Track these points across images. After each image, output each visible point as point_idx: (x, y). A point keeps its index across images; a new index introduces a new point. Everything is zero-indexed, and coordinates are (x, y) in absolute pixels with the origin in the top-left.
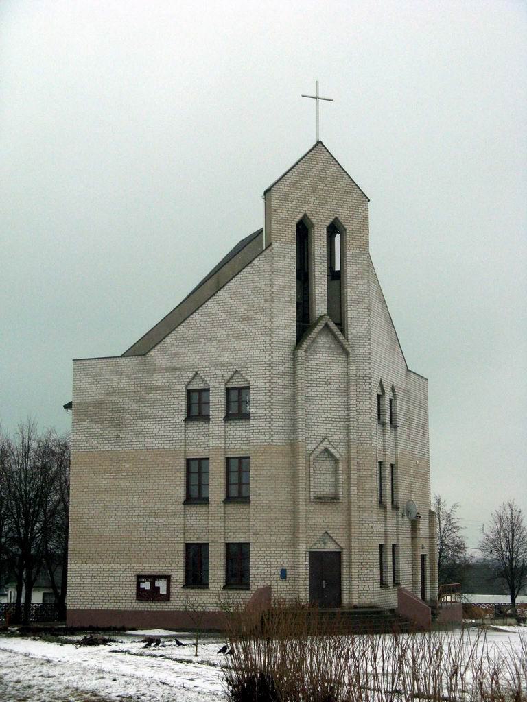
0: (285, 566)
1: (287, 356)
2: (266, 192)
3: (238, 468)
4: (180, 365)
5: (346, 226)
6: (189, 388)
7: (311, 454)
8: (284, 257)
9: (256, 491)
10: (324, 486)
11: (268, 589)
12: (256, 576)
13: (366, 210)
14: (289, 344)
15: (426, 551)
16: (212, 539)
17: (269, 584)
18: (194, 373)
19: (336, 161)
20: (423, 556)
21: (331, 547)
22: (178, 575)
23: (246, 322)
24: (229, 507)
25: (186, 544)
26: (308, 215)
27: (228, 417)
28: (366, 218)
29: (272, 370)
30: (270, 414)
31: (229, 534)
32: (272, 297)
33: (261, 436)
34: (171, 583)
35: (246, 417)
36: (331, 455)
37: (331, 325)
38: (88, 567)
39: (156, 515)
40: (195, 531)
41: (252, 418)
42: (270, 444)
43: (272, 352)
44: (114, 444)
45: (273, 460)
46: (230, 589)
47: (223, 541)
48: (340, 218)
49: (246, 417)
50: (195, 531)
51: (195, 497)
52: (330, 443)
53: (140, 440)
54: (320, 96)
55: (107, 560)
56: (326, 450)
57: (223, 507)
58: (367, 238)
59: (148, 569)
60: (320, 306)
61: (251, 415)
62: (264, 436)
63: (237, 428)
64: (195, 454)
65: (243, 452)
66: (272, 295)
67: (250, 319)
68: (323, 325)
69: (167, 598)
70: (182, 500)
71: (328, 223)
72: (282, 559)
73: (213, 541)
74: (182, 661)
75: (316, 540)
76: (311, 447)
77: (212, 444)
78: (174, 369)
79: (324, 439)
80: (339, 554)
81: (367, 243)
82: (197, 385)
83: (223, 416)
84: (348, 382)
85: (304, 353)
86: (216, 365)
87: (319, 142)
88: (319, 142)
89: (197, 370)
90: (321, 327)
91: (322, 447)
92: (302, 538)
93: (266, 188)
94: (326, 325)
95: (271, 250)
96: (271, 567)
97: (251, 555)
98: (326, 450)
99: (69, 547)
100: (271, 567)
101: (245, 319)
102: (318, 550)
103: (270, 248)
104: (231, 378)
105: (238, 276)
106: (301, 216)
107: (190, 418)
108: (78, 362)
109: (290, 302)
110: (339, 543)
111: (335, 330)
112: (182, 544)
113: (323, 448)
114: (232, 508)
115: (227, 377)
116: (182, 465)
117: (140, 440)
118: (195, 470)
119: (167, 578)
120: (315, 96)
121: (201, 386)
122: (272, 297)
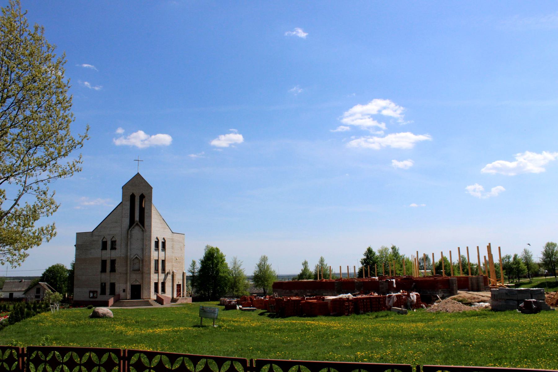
0: (125, 288)
2: (123, 187)
3: (113, 262)
10: (136, 267)
11: (119, 295)
15: (181, 283)
20: (179, 286)
21: (138, 283)
22: (99, 290)
24: (112, 273)
27: (111, 249)
28: (151, 193)
35: (115, 249)
36: (138, 259)
49: (115, 249)
51: (103, 270)
52: (138, 255)
56: (136, 257)
59: (92, 289)
60: (137, 218)
63: (113, 252)
70: (100, 271)
74: (482, 296)
82: (105, 240)
86: (109, 235)
91: (135, 257)
98: (136, 257)
107: (102, 249)
114: (112, 273)
115: (111, 238)
118: (104, 263)
119: (97, 292)
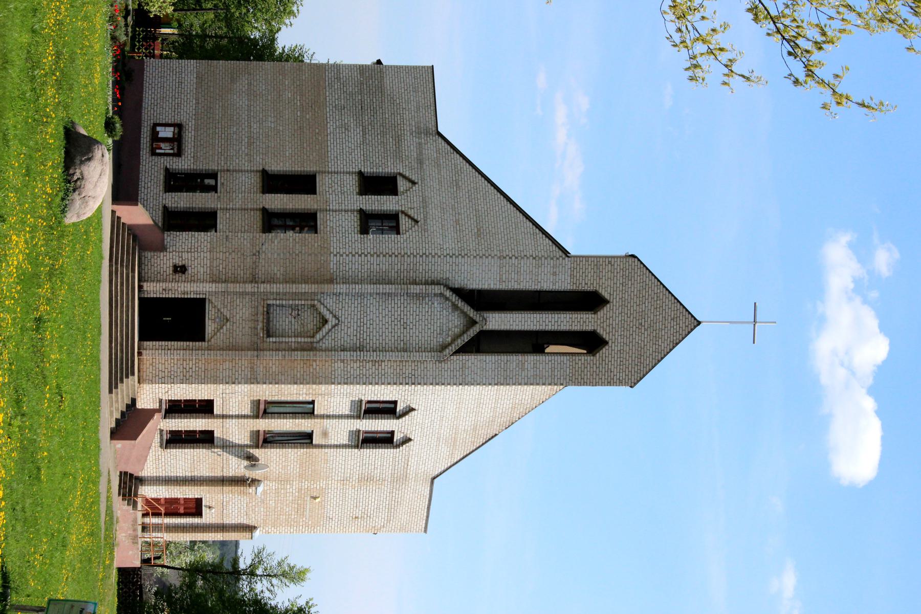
1: (437, 275)
2: (633, 256)
4: (425, 168)
5: (598, 355)
6: (398, 178)
7: (320, 302)
8: (554, 274)
9: (277, 238)
10: (283, 321)
12: (178, 238)
13: (621, 383)
14: (450, 278)
16: (222, 197)
17: (168, 250)
18: (416, 181)
19: (677, 344)
20: (195, 508)
22: (183, 164)
23: (476, 231)
24: (258, 214)
25: (217, 174)
26: (608, 305)
29: (418, 256)
30: (366, 253)
31: (228, 214)
32: (505, 258)
33: (341, 244)
34: (171, 158)
37: (474, 328)
38: (193, 78)
39: (250, 144)
40: (231, 181)
41: (362, 236)
42: (331, 253)
43: (440, 257)
44: (334, 105)
45: (313, 255)
46: (165, 177)
47: (219, 206)
48: (607, 347)
50: (231, 181)
52: (334, 327)
53: (338, 129)
54: (756, 325)
55: (200, 97)
56: (326, 321)
57: (258, 207)
58: (585, 384)
59: (189, 137)
60: (498, 321)
61: (365, 235)
62: (341, 247)
63: (353, 221)
64: (321, 182)
65: (322, 228)
66: (508, 258)
67: (479, 236)
68: (474, 318)
69: (153, 153)
70: (267, 168)
71: (600, 331)
72: (198, 263)
73: (219, 197)
75: (219, 307)
76: (329, 302)
77: (332, 197)
78: (420, 162)
79: (338, 319)
80: (202, 339)
81: (579, 384)
83: (364, 208)
84: (405, 350)
85: (439, 292)
87: (699, 323)
88: (699, 323)
89: (420, 183)
90: (471, 315)
91: (328, 316)
92: (221, 287)
93: (636, 255)
94: (473, 323)
95: (561, 257)
96: (188, 252)
97: (202, 233)
98: (326, 321)
99: (215, 61)
100: (188, 252)
101: (479, 230)
102: (207, 311)
103: (564, 256)
104: (409, 217)
105: (531, 224)
106: (607, 296)
108: (430, 71)
109: (501, 281)
110: (215, 337)
111: (469, 333)
112: (216, 168)
113: (327, 317)
115: (411, 213)
116: (309, 168)
117: (338, 129)
120: (758, 320)
121: (403, 227)
122: (505, 258)
